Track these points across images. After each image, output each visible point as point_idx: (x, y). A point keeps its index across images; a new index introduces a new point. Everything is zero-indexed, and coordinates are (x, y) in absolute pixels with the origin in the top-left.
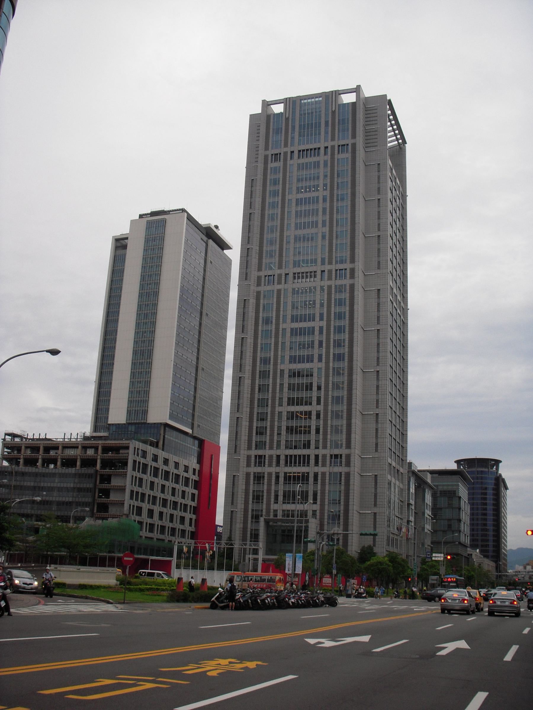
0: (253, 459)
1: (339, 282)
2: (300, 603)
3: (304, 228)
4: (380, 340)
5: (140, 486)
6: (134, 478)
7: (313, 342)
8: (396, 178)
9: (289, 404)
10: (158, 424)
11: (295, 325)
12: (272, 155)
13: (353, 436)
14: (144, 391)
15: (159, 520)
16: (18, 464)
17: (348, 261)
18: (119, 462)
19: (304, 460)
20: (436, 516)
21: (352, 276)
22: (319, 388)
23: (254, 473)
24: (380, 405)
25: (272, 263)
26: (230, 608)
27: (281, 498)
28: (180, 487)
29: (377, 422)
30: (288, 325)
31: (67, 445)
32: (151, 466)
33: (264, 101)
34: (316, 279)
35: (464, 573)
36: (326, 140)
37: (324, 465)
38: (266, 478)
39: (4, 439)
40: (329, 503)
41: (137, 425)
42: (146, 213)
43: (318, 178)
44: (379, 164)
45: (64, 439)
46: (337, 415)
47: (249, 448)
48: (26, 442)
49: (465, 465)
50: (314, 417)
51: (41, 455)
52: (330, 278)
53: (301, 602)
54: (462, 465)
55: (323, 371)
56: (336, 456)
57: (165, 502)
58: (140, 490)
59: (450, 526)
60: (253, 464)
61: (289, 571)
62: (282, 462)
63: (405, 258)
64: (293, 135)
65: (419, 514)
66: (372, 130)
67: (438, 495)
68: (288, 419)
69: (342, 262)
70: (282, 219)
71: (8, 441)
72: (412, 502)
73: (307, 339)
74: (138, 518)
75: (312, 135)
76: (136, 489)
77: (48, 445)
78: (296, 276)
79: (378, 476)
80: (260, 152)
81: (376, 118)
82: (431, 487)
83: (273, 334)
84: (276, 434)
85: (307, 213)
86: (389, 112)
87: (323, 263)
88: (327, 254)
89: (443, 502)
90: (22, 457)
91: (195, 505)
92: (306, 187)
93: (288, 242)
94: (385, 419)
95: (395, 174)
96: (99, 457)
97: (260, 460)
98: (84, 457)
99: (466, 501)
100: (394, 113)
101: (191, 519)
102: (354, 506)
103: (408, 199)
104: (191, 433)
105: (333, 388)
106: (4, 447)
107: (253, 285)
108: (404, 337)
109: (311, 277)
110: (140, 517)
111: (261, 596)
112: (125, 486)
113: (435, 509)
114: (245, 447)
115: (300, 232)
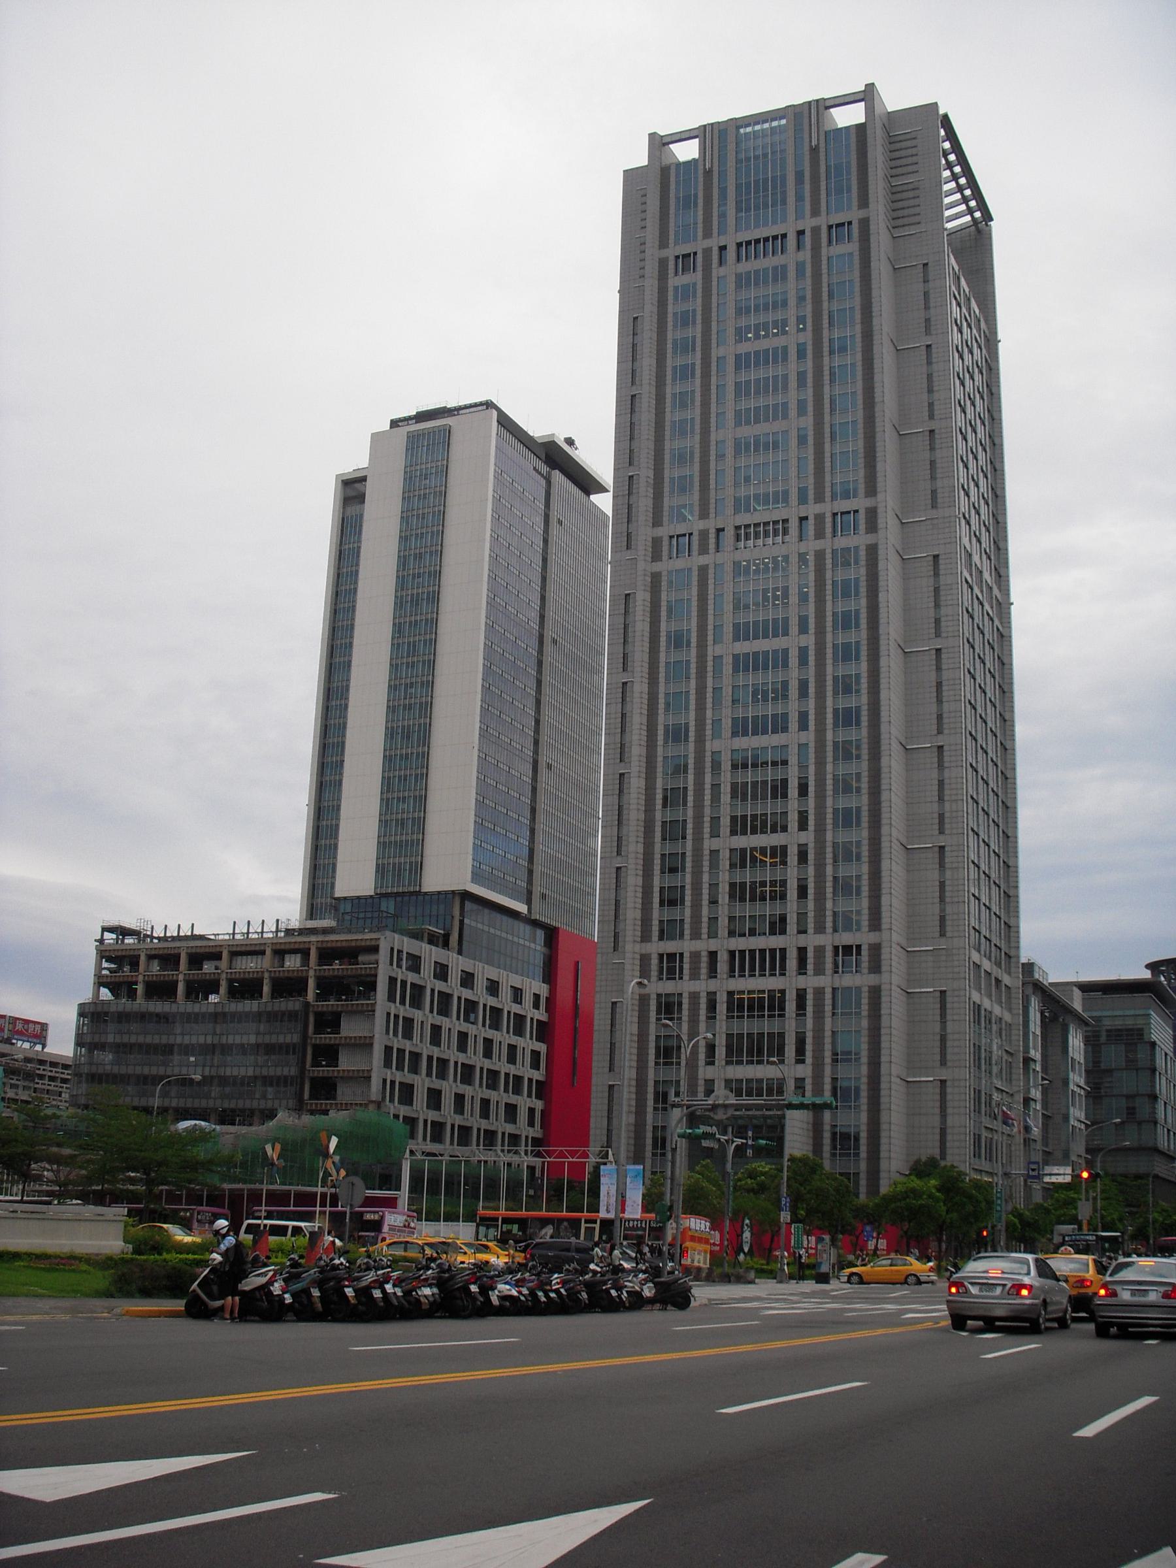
0: (655, 961)
1: (842, 542)
2: (543, 1299)
3: (757, 421)
4: (944, 672)
5: (408, 1035)
7: (785, 684)
8: (969, 299)
9: (733, 832)
10: (446, 893)
11: (743, 647)
12: (677, 257)
13: (885, 900)
14: (414, 819)
15: (455, 1112)
16: (132, 994)
18: (359, 984)
19: (773, 961)
20: (1099, 1088)
21: (872, 527)
22: (803, 790)
23: (659, 996)
24: (947, 826)
25: (684, 506)
26: (228, 1316)
27: (721, 1052)
28: (503, 1037)
29: (942, 865)
30: (726, 648)
31: (238, 949)
32: (459, 998)
33: (653, 136)
34: (787, 538)
35: (1153, 1218)
36: (799, 215)
37: (819, 971)
38: (685, 1006)
39: (101, 941)
41: (399, 899)
42: (406, 415)
43: (785, 303)
44: (925, 265)
45: (234, 934)
46: (846, 854)
47: (645, 937)
48: (151, 946)
49: (1169, 974)
50: (793, 859)
51: (182, 974)
52: (820, 535)
53: (547, 1296)
54: (1162, 972)
55: (812, 750)
56: (848, 949)
57: (467, 1074)
58: (408, 1046)
59: (1131, 1111)
60: (654, 973)
61: (608, 1211)
62: (722, 966)
63: (999, 486)
64: (722, 208)
65: (1055, 1086)
66: (905, 188)
67: (1103, 1039)
68: (733, 866)
69: (846, 495)
70: (705, 404)
71: (110, 944)
72: (1035, 1054)
73: (771, 678)
74: (404, 1111)
75: (766, 206)
76: (398, 1043)
77: (198, 950)
78: (742, 533)
79: (948, 993)
80: (649, 252)
81: (914, 158)
82: (1081, 1021)
83: (693, 670)
84: (705, 902)
85: (762, 387)
86: (947, 145)
87: (803, 499)
88: (811, 480)
89: (1113, 1055)
90: (141, 978)
91: (541, 1078)
92: (757, 327)
93: (721, 457)
94: (960, 859)
95: (967, 290)
96: (311, 973)
97: (671, 965)
98: (277, 975)
99: (1168, 1052)
100: (957, 148)
101: (532, 1111)
102: (893, 1065)
103: (1001, 347)
104: (526, 912)
105: (835, 791)
106: (102, 957)
107: (642, 558)
108: (1003, 669)
109: (776, 533)
110: (438, 1113)
111: (358, 1279)
112: (372, 1037)
113: (1096, 1072)
114: (634, 936)
115: (747, 432)
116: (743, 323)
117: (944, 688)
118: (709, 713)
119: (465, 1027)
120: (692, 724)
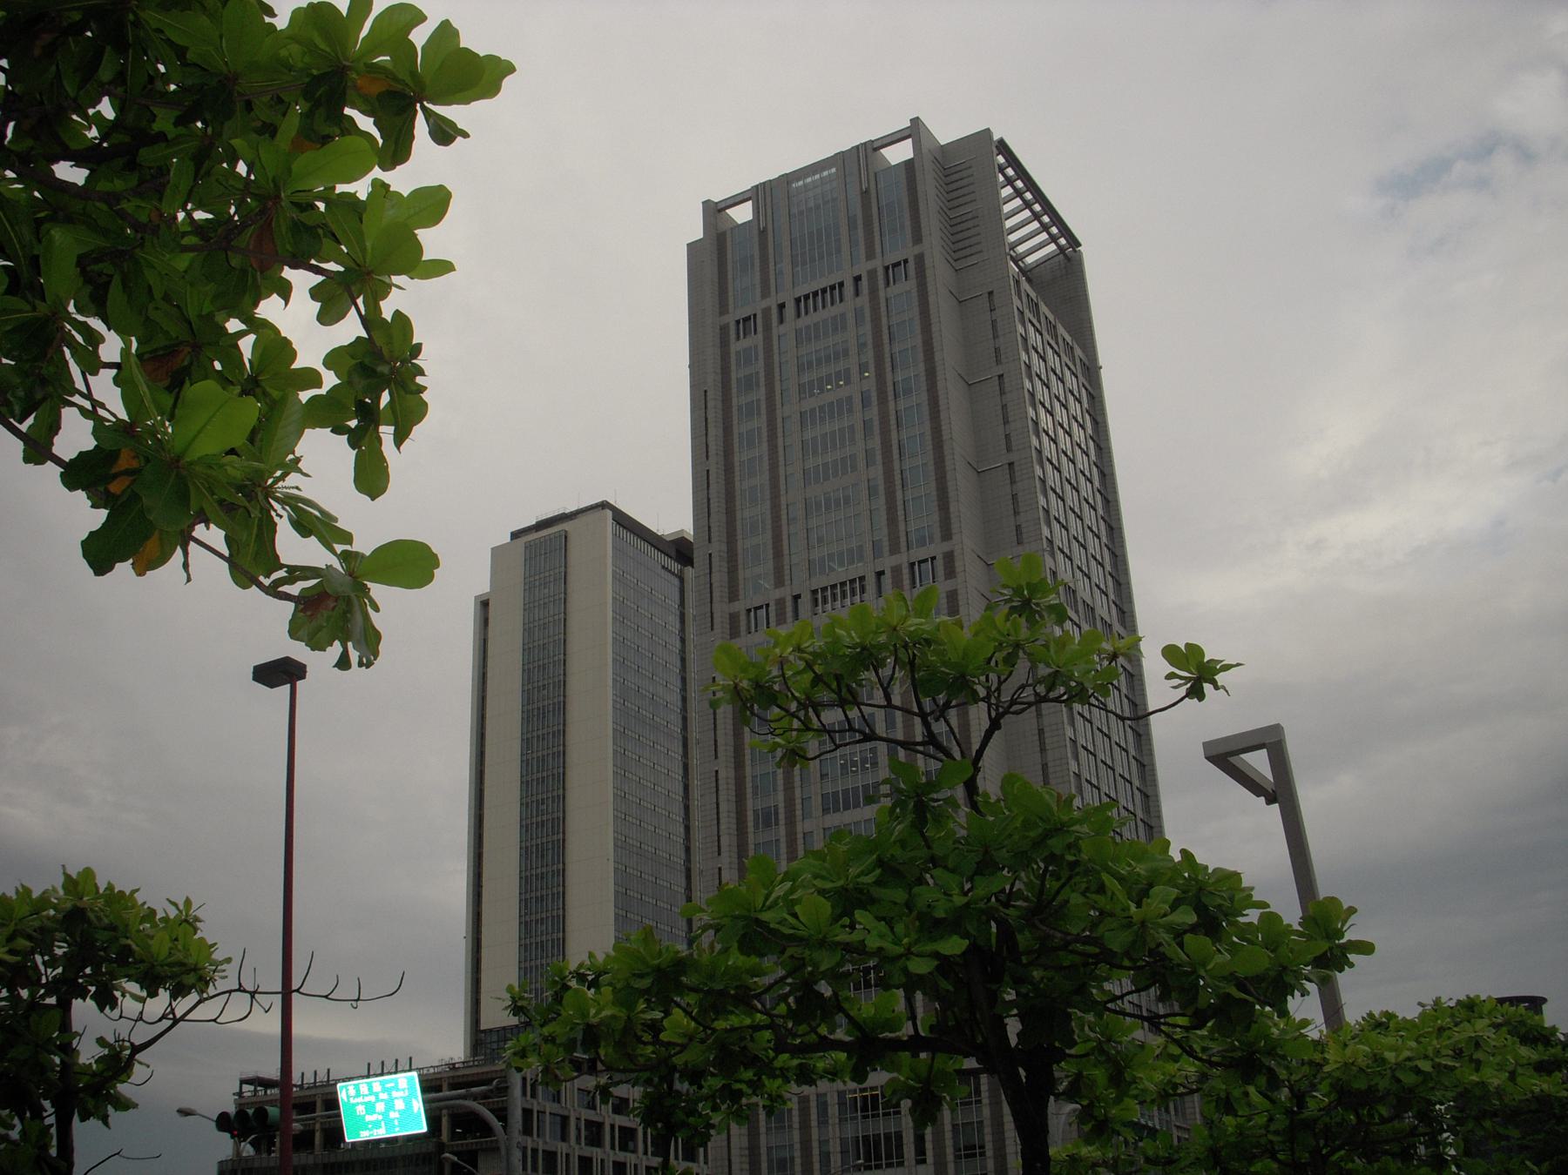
6: (529, 1152)
12: (738, 322)
17: (937, 535)
39: (240, 1094)
40: (957, 1157)
43: (846, 353)
44: (991, 293)
69: (922, 542)
81: (971, 187)
103: (1105, 376)
116: (805, 379)
117: (1046, 735)
118: (798, 792)
119: (621, 1156)
120: (781, 806)
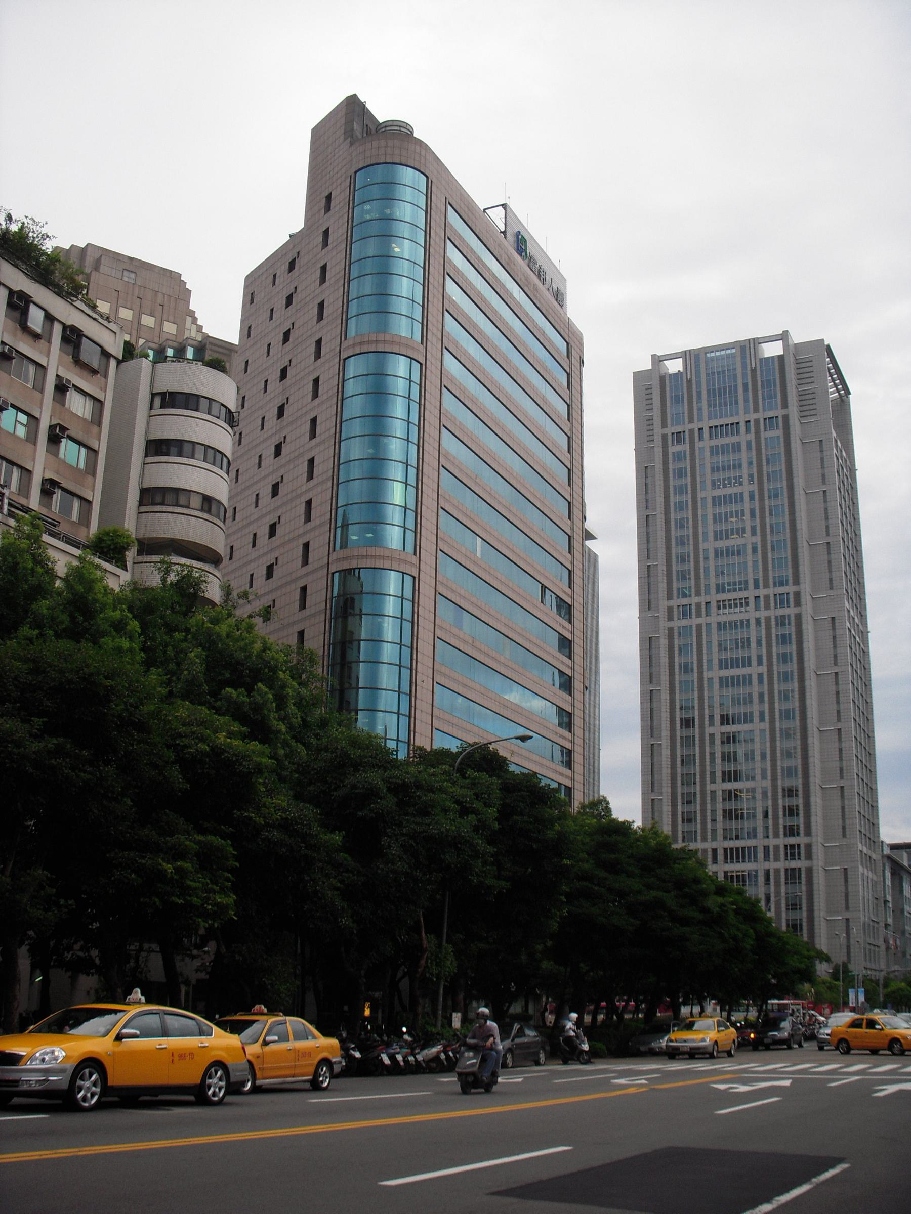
43: (740, 466)
